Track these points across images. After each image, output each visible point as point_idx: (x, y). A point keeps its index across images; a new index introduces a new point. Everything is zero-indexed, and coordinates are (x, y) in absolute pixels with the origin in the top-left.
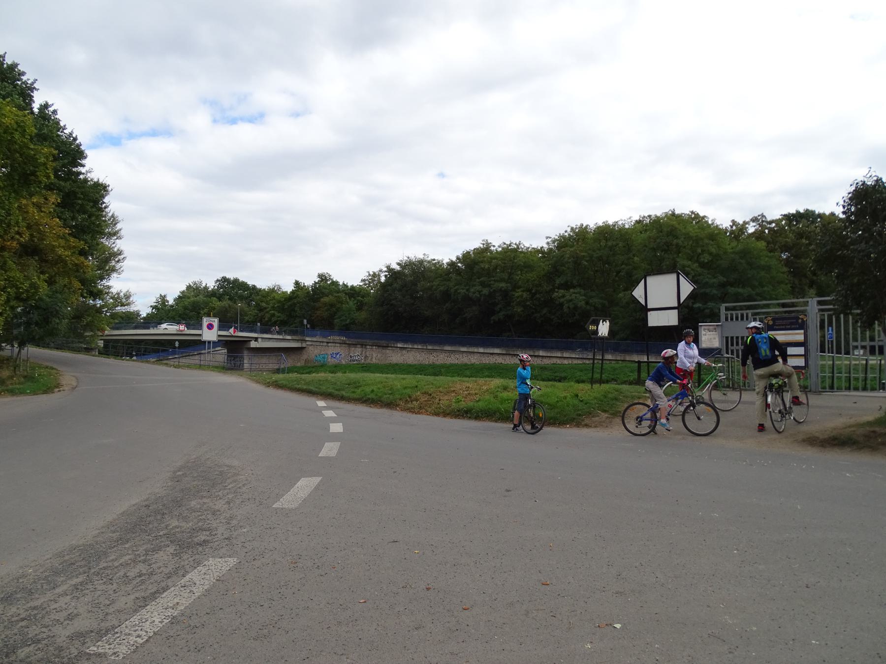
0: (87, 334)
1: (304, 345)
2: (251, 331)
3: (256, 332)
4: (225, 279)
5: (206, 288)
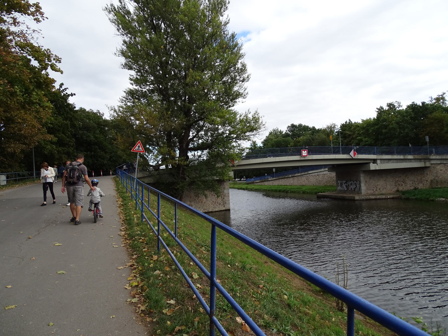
0: (218, 165)
1: (428, 164)
2: (369, 153)
3: (374, 154)
4: (293, 126)
5: (281, 132)
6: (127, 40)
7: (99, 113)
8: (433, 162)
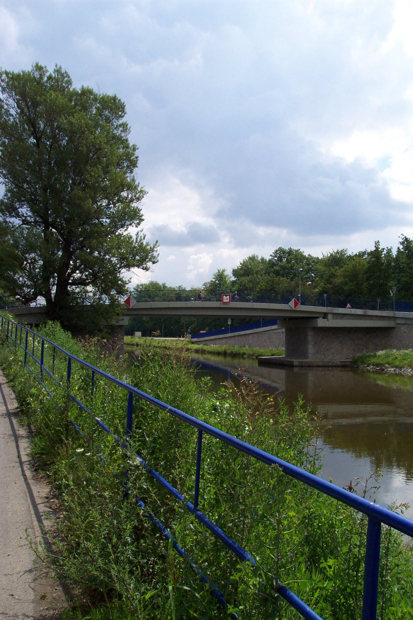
6: (135, 278)
7: (348, 271)
8: (399, 321)
